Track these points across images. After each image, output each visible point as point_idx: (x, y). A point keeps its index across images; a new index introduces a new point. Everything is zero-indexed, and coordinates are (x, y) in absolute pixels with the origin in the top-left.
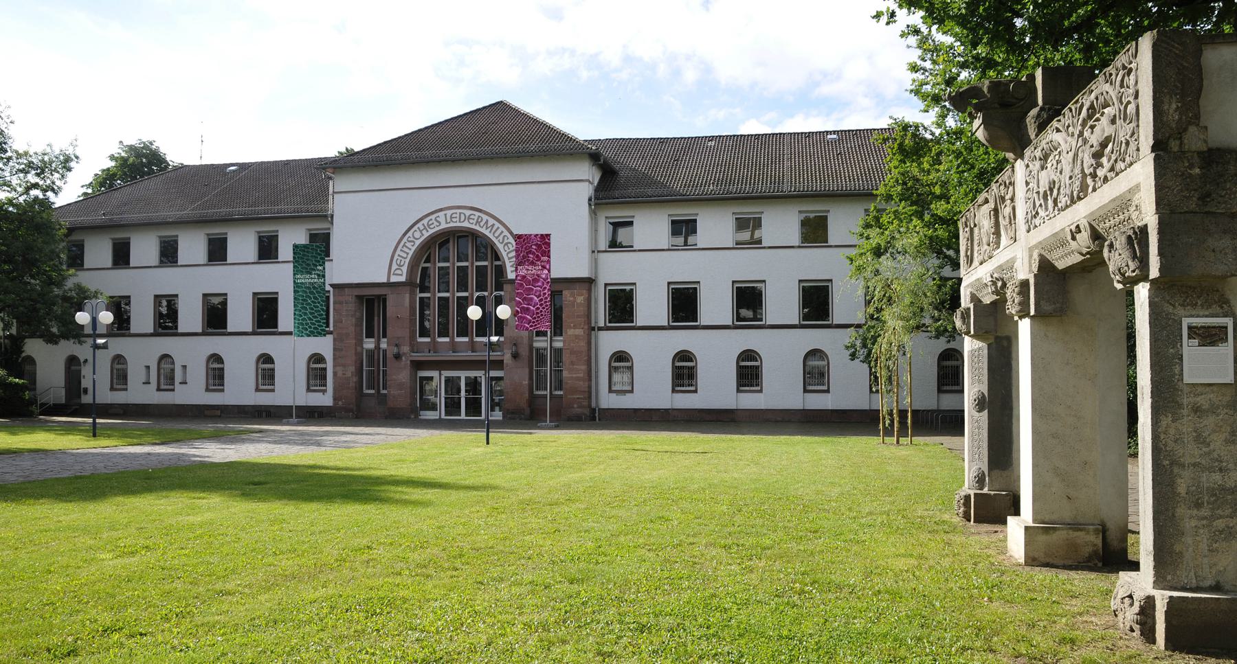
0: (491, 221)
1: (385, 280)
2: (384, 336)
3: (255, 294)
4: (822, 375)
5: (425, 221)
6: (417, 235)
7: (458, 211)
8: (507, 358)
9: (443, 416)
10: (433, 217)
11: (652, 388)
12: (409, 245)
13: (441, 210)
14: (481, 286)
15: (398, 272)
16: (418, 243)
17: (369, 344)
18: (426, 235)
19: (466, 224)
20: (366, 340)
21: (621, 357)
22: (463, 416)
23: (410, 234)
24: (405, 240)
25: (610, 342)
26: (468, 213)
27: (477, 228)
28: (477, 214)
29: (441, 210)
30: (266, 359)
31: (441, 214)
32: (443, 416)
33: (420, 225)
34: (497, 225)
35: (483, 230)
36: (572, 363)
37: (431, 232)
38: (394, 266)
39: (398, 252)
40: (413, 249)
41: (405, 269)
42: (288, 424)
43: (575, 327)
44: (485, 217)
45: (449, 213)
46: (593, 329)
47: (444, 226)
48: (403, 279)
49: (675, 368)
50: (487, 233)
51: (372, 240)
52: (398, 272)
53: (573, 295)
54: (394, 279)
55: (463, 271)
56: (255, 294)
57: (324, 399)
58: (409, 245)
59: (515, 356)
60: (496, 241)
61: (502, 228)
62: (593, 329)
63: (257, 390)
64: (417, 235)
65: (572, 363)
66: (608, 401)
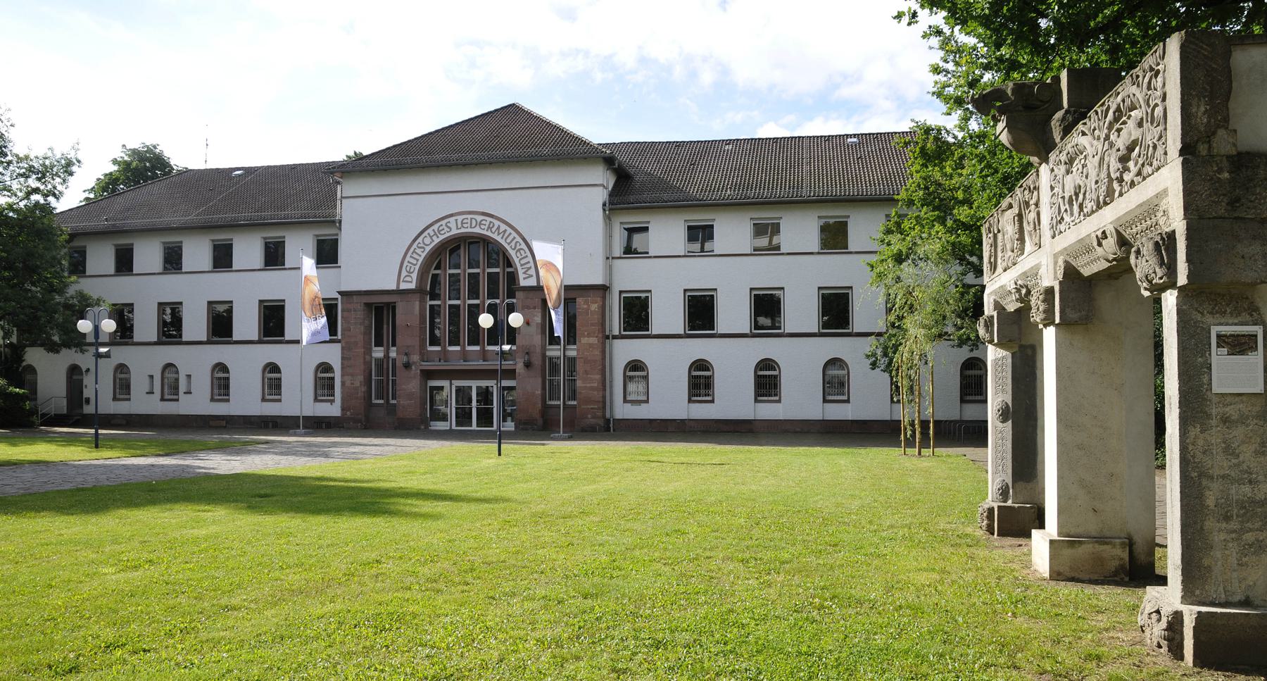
0: (503, 227)
1: (394, 288)
2: (394, 345)
3: (261, 302)
4: (842, 384)
5: (435, 227)
6: (427, 241)
7: (469, 216)
8: (520, 367)
9: (454, 427)
10: (443, 222)
11: (668, 398)
12: (419, 251)
13: (451, 215)
14: (493, 294)
15: (408, 279)
16: (428, 249)
17: (378, 353)
18: (437, 241)
19: (477, 230)
20: (375, 349)
21: (636, 366)
22: (474, 427)
23: (420, 240)
24: (415, 246)
25: (625, 350)
26: (479, 218)
27: (489, 234)
28: (489, 219)
29: (451, 215)
30: (273, 368)
31: (452, 219)
32: (454, 427)
33: (430, 231)
34: (509, 230)
35: (495, 236)
36: (586, 372)
37: (442, 237)
38: (404, 273)
39: (408, 258)
40: (423, 255)
41: (415, 276)
42: (295, 435)
43: (589, 336)
44: (497, 223)
45: (460, 218)
46: (608, 337)
47: (454, 232)
48: (412, 286)
49: (691, 378)
50: (498, 238)
51: (384, 244)
52: (408, 279)
53: (586, 302)
54: (403, 286)
55: (474, 278)
56: (261, 302)
57: (332, 409)
58: (419, 251)
59: (528, 365)
60: (508, 247)
61: (514, 234)
62: (608, 337)
63: (264, 400)
64: (427, 241)
65: (586, 372)
66: (623, 411)
